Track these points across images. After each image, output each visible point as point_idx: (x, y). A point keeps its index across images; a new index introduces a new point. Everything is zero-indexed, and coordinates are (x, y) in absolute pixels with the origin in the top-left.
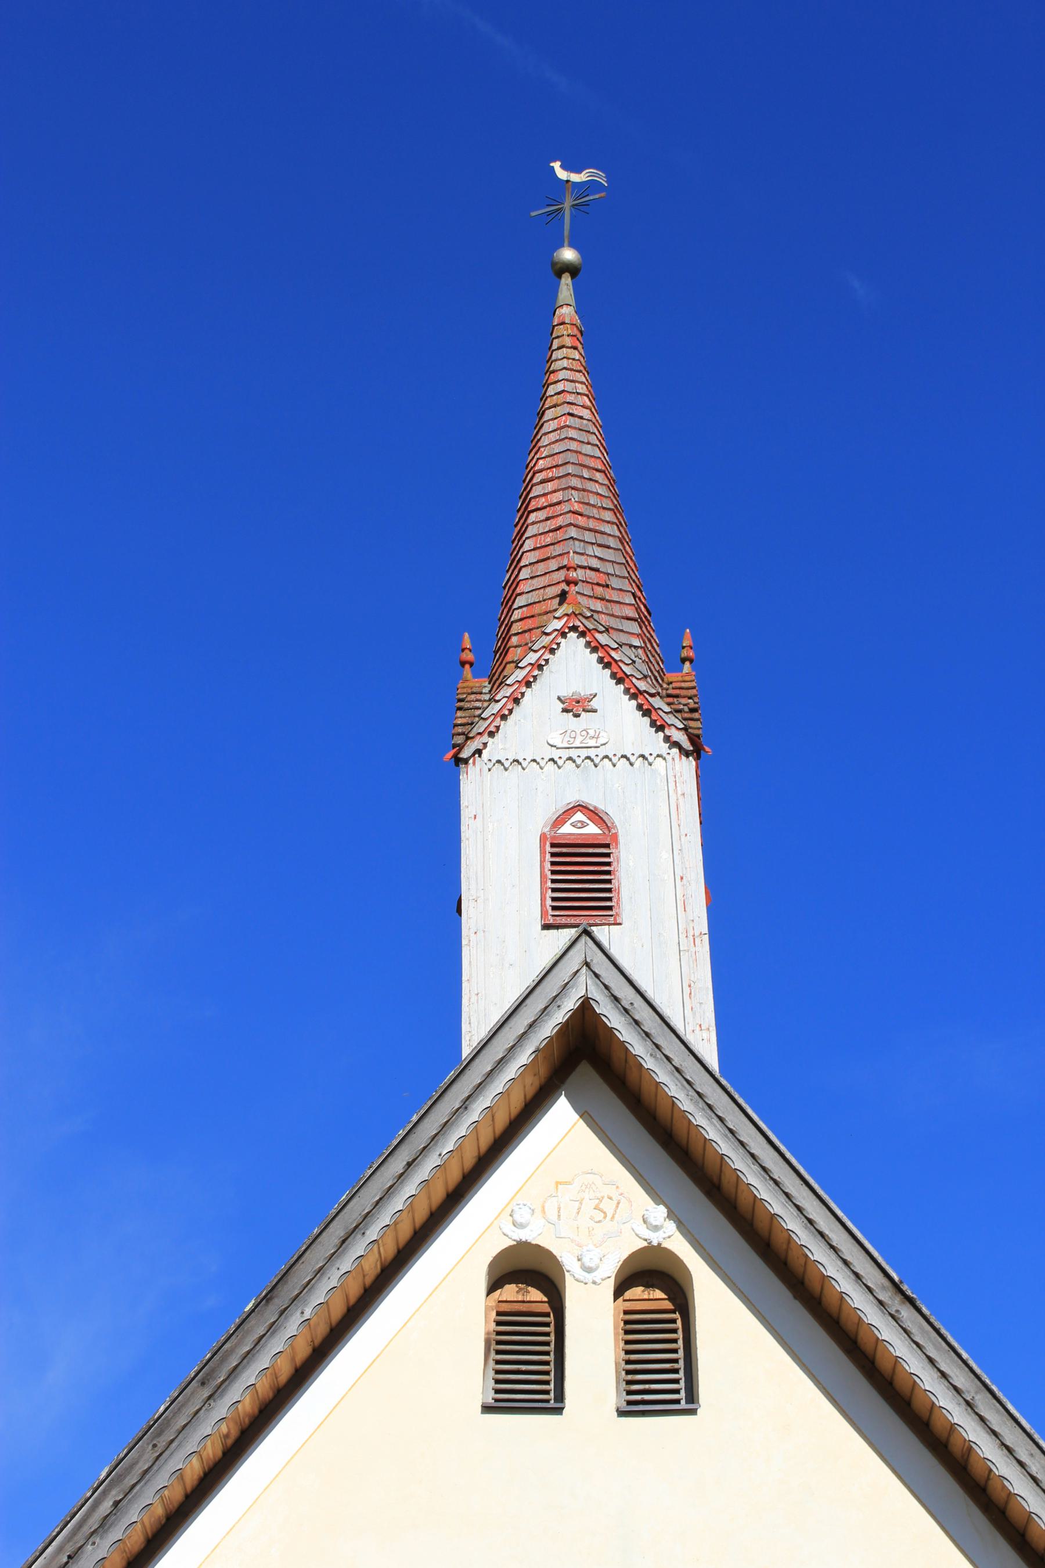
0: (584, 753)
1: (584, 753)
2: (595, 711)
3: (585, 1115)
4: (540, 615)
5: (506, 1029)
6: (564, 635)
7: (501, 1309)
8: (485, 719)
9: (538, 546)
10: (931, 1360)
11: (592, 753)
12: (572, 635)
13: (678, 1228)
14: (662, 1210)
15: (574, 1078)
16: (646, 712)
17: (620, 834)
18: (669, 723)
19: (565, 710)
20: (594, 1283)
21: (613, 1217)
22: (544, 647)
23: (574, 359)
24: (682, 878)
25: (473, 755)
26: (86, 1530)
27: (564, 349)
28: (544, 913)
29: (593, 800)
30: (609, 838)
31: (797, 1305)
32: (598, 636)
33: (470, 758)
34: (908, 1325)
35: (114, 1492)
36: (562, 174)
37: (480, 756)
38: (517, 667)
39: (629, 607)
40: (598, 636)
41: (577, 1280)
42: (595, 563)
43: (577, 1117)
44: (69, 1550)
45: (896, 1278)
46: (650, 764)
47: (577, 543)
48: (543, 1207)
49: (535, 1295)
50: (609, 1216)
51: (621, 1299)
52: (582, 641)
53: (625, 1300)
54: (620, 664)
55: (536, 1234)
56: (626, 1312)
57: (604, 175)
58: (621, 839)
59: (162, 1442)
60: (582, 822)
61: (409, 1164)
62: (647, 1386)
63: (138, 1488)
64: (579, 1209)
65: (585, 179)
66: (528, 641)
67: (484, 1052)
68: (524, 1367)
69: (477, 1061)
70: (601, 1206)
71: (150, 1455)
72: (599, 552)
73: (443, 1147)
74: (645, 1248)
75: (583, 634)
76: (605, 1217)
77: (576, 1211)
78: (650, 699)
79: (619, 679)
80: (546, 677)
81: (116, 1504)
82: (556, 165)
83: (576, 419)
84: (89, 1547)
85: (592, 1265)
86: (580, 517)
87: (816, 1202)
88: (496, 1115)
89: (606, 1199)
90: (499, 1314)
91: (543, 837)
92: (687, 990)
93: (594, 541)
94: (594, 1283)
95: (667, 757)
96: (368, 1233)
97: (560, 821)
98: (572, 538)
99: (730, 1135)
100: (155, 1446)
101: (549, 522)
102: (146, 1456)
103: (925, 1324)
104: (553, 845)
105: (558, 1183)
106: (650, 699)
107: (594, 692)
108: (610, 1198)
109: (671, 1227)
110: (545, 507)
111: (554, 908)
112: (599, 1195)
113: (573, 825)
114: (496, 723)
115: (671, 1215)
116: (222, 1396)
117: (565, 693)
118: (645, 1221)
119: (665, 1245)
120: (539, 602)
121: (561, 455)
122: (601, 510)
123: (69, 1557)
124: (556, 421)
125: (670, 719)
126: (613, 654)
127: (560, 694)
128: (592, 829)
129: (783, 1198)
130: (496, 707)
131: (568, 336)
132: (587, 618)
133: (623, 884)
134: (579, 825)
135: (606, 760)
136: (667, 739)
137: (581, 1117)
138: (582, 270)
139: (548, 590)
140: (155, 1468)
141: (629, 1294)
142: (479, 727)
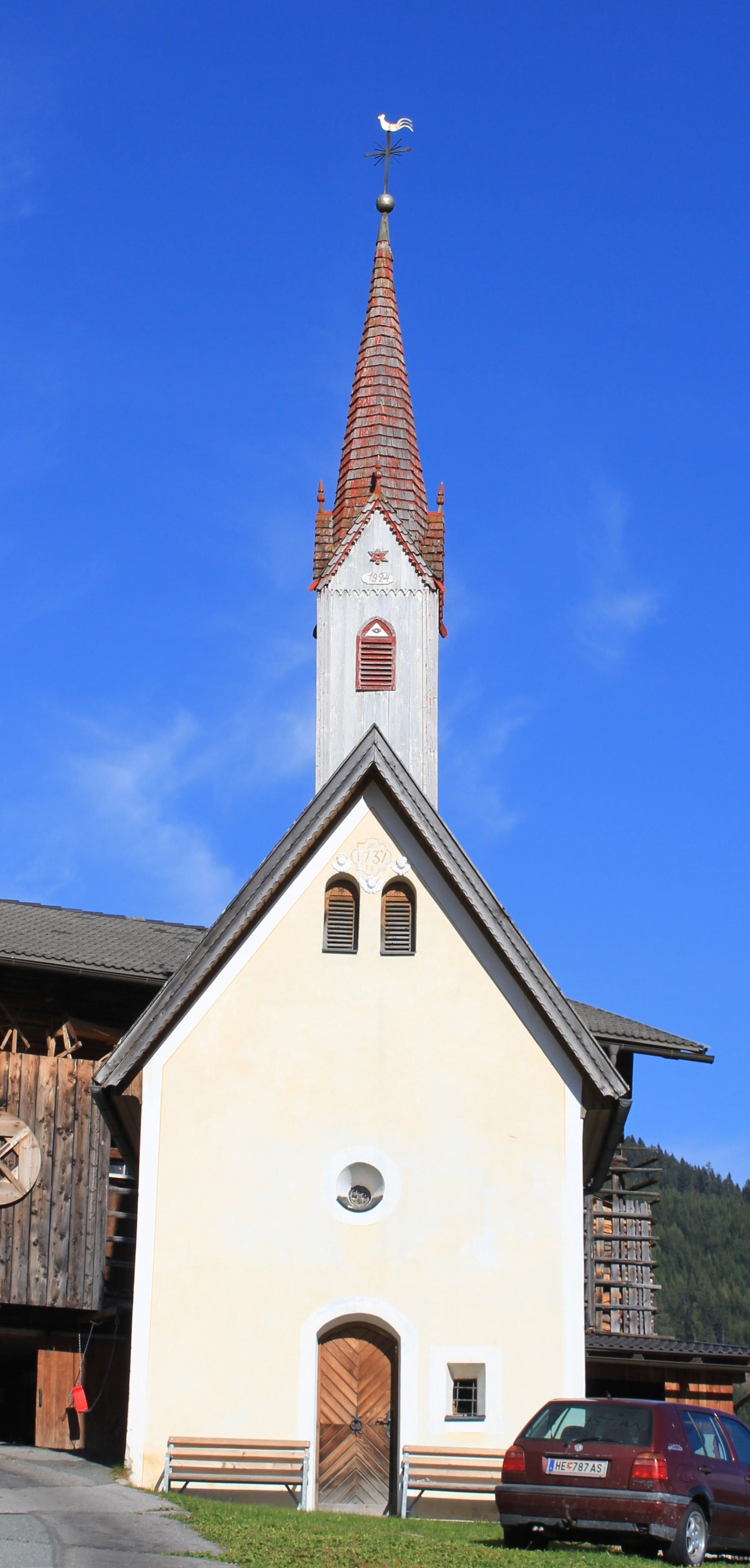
0: (380, 588)
1: (380, 588)
2: (387, 561)
3: (372, 808)
4: (361, 488)
5: (337, 778)
6: (372, 512)
7: (331, 899)
8: (330, 566)
9: (362, 436)
10: (513, 944)
11: (384, 587)
12: (377, 512)
13: (412, 867)
14: (405, 859)
15: (367, 790)
16: (414, 564)
17: (397, 637)
18: (425, 572)
19: (372, 561)
20: (373, 893)
21: (382, 861)
23: (386, 288)
24: (426, 665)
26: (160, 1008)
27: (381, 279)
28: (357, 683)
29: (384, 617)
30: (391, 640)
31: (462, 906)
32: (391, 515)
34: (505, 928)
35: (170, 992)
36: (386, 126)
37: (327, 587)
38: (347, 533)
39: (409, 482)
40: (391, 515)
41: (366, 892)
42: (392, 452)
43: (367, 809)
44: (153, 1016)
45: (502, 907)
46: (414, 595)
47: (383, 437)
48: (351, 855)
49: (347, 893)
50: (381, 860)
51: (385, 896)
52: (382, 516)
53: (387, 896)
54: (401, 534)
55: (348, 868)
56: (387, 902)
57: (411, 121)
59: (189, 970)
60: (378, 630)
61: (292, 845)
62: (395, 937)
63: (179, 990)
66: (354, 505)
67: (327, 789)
69: (323, 793)
70: (378, 855)
71: (184, 976)
72: (393, 442)
73: (307, 836)
75: (382, 512)
76: (379, 861)
77: (366, 857)
78: (416, 557)
79: (401, 542)
81: (171, 997)
82: (382, 118)
83: (386, 338)
84: (161, 1014)
85: (372, 886)
86: (385, 417)
87: (471, 869)
89: (380, 852)
91: (358, 638)
92: (425, 730)
93: (392, 435)
94: (373, 893)
95: (423, 592)
96: (274, 877)
97: (366, 629)
98: (380, 435)
99: (435, 835)
100: (186, 972)
101: (368, 418)
102: (182, 977)
103: (512, 927)
104: (363, 643)
105: (358, 843)
106: (416, 557)
108: (382, 851)
109: (408, 867)
110: (366, 407)
111: (362, 680)
112: (377, 850)
113: (374, 631)
114: (335, 569)
115: (409, 861)
116: (213, 951)
117: (372, 550)
118: (397, 864)
119: (405, 875)
120: (361, 478)
121: (376, 367)
122: (397, 409)
123: (154, 1019)
124: (374, 338)
125: (425, 570)
126: (398, 527)
127: (369, 550)
128: (383, 634)
129: (456, 867)
130: (337, 558)
131: (384, 267)
132: (385, 503)
133: (397, 667)
135: (392, 592)
136: (423, 581)
137: (370, 809)
138: (394, 209)
139: (366, 470)
140: (186, 982)
141: (388, 894)
142: (327, 571)
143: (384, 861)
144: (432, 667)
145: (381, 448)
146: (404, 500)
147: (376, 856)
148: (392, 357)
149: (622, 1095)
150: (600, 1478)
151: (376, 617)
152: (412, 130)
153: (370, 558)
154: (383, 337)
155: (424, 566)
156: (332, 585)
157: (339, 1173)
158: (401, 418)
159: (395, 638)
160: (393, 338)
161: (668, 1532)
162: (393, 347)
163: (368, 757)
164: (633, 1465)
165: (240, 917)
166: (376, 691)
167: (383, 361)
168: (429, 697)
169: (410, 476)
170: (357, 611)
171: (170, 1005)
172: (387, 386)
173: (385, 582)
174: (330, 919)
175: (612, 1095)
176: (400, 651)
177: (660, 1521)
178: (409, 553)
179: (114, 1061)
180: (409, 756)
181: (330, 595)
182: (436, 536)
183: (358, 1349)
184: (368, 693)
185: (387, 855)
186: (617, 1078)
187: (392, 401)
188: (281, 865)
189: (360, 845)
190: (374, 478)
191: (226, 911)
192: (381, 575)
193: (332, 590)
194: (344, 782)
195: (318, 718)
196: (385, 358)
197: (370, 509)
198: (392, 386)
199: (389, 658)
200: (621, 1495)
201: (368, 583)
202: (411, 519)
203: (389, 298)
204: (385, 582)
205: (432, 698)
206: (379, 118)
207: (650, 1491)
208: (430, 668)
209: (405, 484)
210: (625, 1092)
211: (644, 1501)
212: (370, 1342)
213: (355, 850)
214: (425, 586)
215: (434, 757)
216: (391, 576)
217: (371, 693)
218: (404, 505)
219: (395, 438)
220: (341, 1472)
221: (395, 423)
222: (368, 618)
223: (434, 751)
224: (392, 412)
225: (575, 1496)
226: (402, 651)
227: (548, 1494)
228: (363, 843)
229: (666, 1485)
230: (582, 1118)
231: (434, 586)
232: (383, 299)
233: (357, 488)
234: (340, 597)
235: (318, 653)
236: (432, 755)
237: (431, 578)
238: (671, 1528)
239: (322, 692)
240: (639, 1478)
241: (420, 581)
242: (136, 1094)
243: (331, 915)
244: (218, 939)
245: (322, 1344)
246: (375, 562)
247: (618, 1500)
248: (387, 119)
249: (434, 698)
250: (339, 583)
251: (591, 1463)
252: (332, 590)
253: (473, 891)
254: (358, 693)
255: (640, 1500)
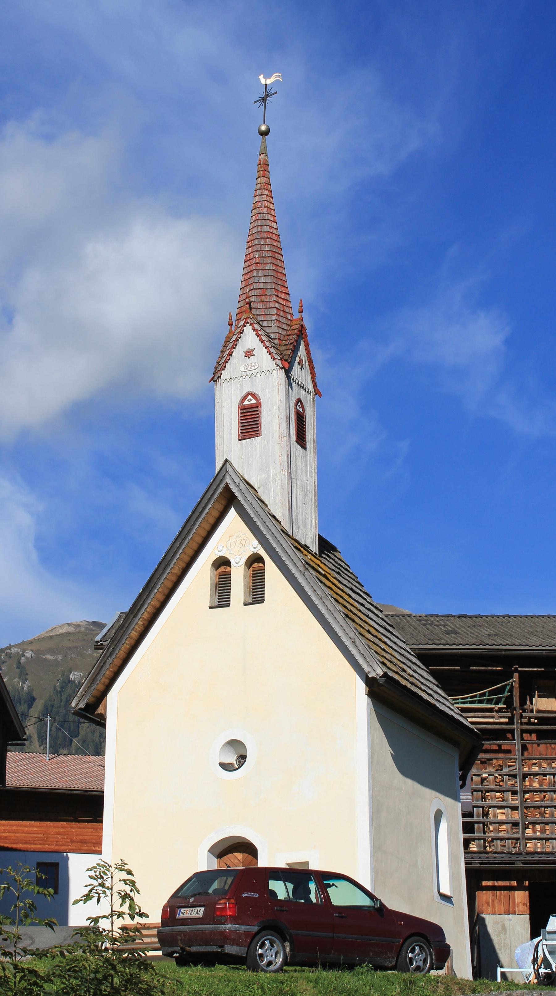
5: (205, 497)
13: (262, 546)
17: (262, 402)
19: (246, 356)
21: (244, 546)
22: (238, 333)
23: (262, 183)
25: (218, 378)
32: (255, 325)
33: (217, 380)
37: (220, 378)
39: (273, 302)
41: (234, 566)
42: (262, 286)
43: (236, 513)
47: (256, 277)
50: (244, 545)
52: (251, 327)
55: (224, 553)
57: (281, 75)
58: (262, 404)
61: (180, 543)
64: (236, 544)
65: (272, 81)
68: (225, 591)
70: (242, 542)
72: (263, 279)
74: (253, 554)
75: (250, 325)
80: (240, 343)
81: (113, 649)
84: (108, 660)
86: (258, 264)
88: (209, 521)
89: (243, 540)
90: (219, 576)
105: (230, 536)
107: (253, 348)
108: (244, 539)
109: (260, 546)
112: (241, 539)
113: (248, 401)
119: (258, 552)
123: (103, 663)
128: (254, 401)
134: (250, 400)
137: (237, 513)
141: (253, 566)
143: (245, 545)
144: (282, 417)
145: (255, 284)
146: (269, 314)
147: (240, 543)
148: (265, 226)
149: (380, 675)
150: (199, 918)
151: (249, 392)
152: (281, 80)
153: (245, 354)
154: (259, 214)
155: (275, 354)
156: (223, 376)
157: (220, 748)
158: (269, 263)
159: (260, 403)
160: (266, 213)
161: (238, 950)
162: (266, 219)
163: (224, 481)
164: (215, 908)
165: (151, 593)
166: (250, 438)
167: (259, 229)
168: (281, 437)
169: (274, 298)
170: (238, 390)
171: (113, 654)
172: (261, 244)
173: (253, 368)
174: (219, 587)
175: (375, 676)
176: (264, 411)
177: (231, 943)
178: (266, 347)
179: (81, 693)
180: (270, 476)
181: (222, 383)
182: (292, 333)
183: (242, 860)
184: (246, 440)
185: (247, 541)
186: (377, 665)
187: (263, 253)
188: (174, 557)
189: (231, 537)
190: (249, 303)
191: (143, 591)
192: (251, 365)
193: (223, 379)
194: (210, 500)
195: (216, 462)
196: (260, 227)
197: (242, 324)
198: (264, 244)
199: (257, 416)
200: (207, 928)
201: (244, 371)
202: (273, 326)
203: (264, 189)
204: (253, 368)
205: (283, 437)
206: (259, 77)
207: (224, 924)
208: (281, 418)
209: (270, 304)
210: (382, 673)
211: (219, 931)
212: (249, 854)
213: (228, 541)
214: (277, 366)
215: (285, 475)
216: (257, 364)
217: (247, 440)
218: (269, 318)
219: (265, 276)
220: (165, 933)
221: (264, 267)
222: (245, 392)
223: (285, 471)
224: (264, 260)
225: (187, 931)
226: (265, 410)
227: (176, 931)
228: (233, 536)
229: (234, 920)
230: (366, 694)
231: (281, 365)
232: (260, 190)
233: (241, 313)
234: (229, 383)
235: (216, 421)
236: (284, 473)
237: (279, 361)
238: (241, 948)
239: (218, 445)
240: (218, 916)
241: (274, 363)
242: (103, 712)
243: (220, 584)
244: (139, 608)
245: (220, 858)
246: (247, 357)
247: (206, 931)
248: (264, 77)
249: (284, 437)
250: (227, 374)
251: (196, 909)
252: (223, 379)
253: (287, 555)
254: (240, 441)
255: (216, 930)
